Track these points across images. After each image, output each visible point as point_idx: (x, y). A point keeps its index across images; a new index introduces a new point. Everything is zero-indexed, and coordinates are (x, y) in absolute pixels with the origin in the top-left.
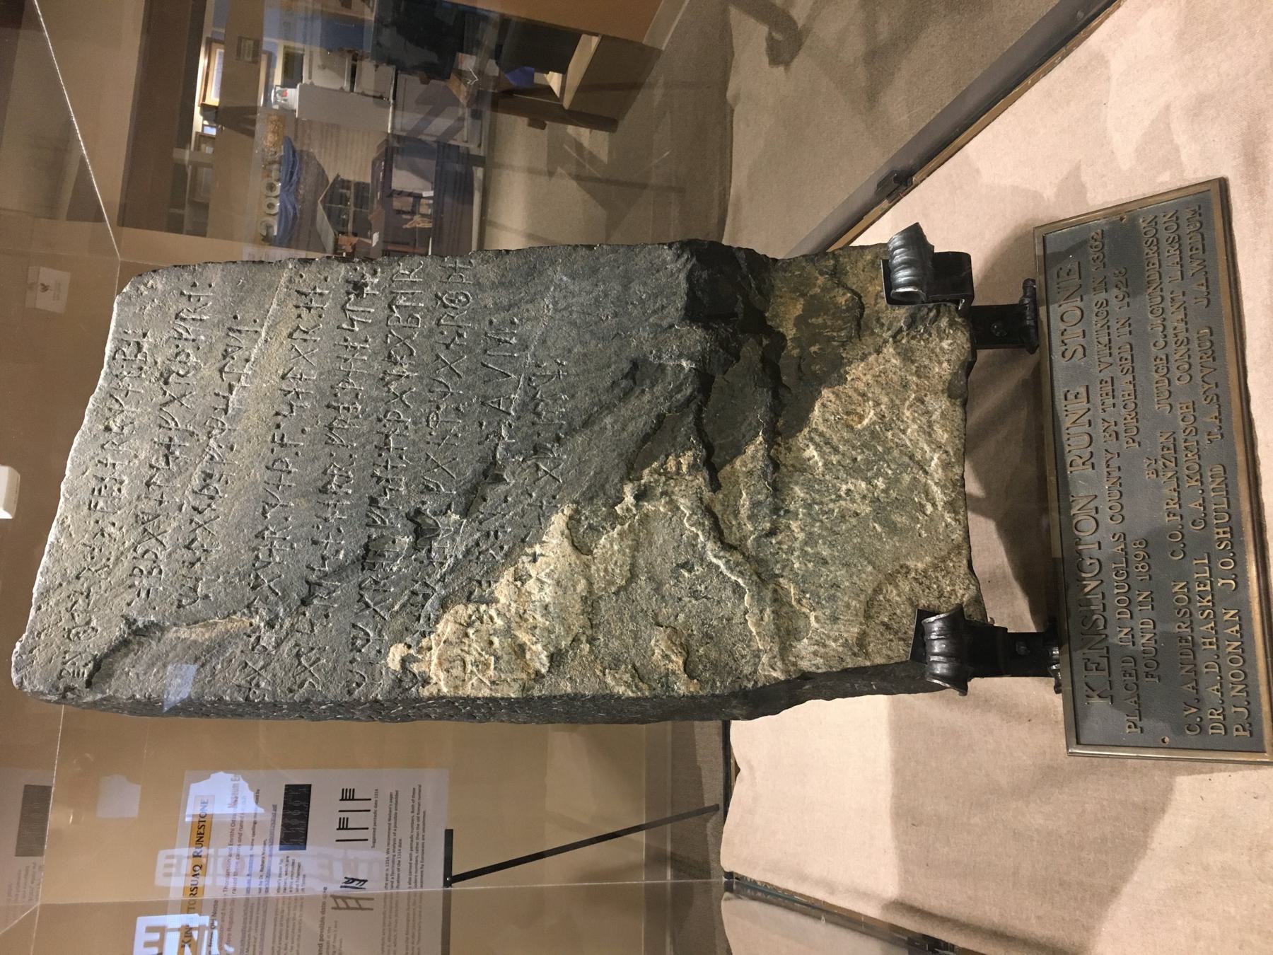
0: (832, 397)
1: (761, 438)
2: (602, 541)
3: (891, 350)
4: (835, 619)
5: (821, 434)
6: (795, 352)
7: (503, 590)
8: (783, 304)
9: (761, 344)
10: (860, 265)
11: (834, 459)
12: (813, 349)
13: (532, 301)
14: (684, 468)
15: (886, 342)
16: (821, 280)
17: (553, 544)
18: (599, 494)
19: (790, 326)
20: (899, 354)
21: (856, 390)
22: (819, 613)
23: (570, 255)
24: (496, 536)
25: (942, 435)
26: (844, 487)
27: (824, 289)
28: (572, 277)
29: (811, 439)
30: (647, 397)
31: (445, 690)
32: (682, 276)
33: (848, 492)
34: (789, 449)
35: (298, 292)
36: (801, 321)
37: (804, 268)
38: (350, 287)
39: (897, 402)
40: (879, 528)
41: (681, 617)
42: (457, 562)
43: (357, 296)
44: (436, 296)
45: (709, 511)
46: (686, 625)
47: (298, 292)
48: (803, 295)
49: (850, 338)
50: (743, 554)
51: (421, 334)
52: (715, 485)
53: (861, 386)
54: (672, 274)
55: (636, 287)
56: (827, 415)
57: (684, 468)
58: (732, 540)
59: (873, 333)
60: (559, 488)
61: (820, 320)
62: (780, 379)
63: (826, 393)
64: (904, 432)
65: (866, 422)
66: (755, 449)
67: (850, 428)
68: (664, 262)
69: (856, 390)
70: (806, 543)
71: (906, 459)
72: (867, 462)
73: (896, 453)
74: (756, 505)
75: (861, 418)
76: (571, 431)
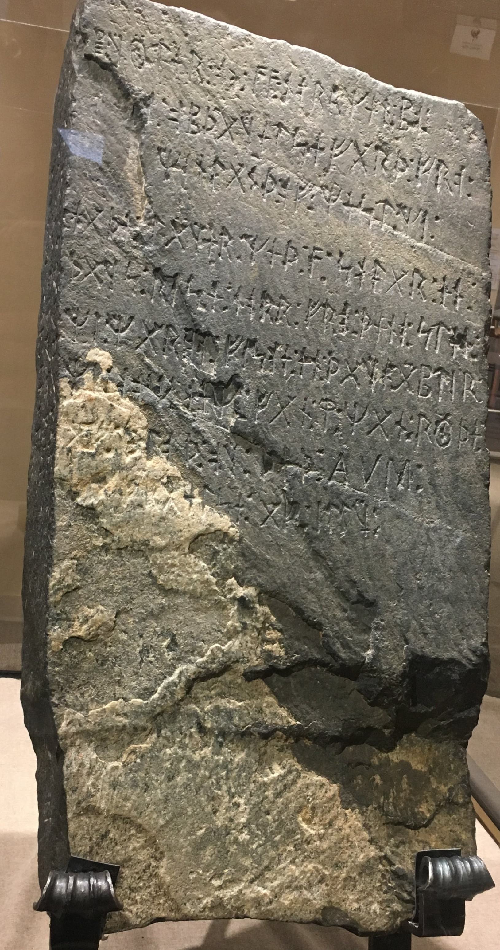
0: (330, 794)
1: (293, 722)
3: (373, 854)
4: (114, 785)
5: (294, 782)
7: (159, 464)
8: (423, 751)
14: (268, 647)
15: (381, 849)
16: (444, 789)
17: (201, 516)
19: (402, 757)
20: (369, 861)
21: (336, 818)
23: (481, 546)
25: (287, 899)
26: (242, 801)
27: (435, 792)
28: (460, 548)
29: (290, 772)
32: (454, 654)
33: (238, 805)
34: (281, 750)
36: (405, 767)
37: (457, 773)
39: (322, 857)
44: (448, 415)
45: (225, 668)
47: (459, 280)
48: (430, 771)
49: (386, 814)
50: (182, 700)
52: (251, 676)
53: (339, 823)
54: (457, 645)
59: (390, 836)
60: (256, 525)
61: (405, 786)
63: (334, 788)
64: (293, 862)
65: (304, 826)
66: (284, 717)
67: (299, 810)
68: (470, 638)
69: (336, 818)
70: (189, 761)
72: (265, 825)
74: (229, 714)
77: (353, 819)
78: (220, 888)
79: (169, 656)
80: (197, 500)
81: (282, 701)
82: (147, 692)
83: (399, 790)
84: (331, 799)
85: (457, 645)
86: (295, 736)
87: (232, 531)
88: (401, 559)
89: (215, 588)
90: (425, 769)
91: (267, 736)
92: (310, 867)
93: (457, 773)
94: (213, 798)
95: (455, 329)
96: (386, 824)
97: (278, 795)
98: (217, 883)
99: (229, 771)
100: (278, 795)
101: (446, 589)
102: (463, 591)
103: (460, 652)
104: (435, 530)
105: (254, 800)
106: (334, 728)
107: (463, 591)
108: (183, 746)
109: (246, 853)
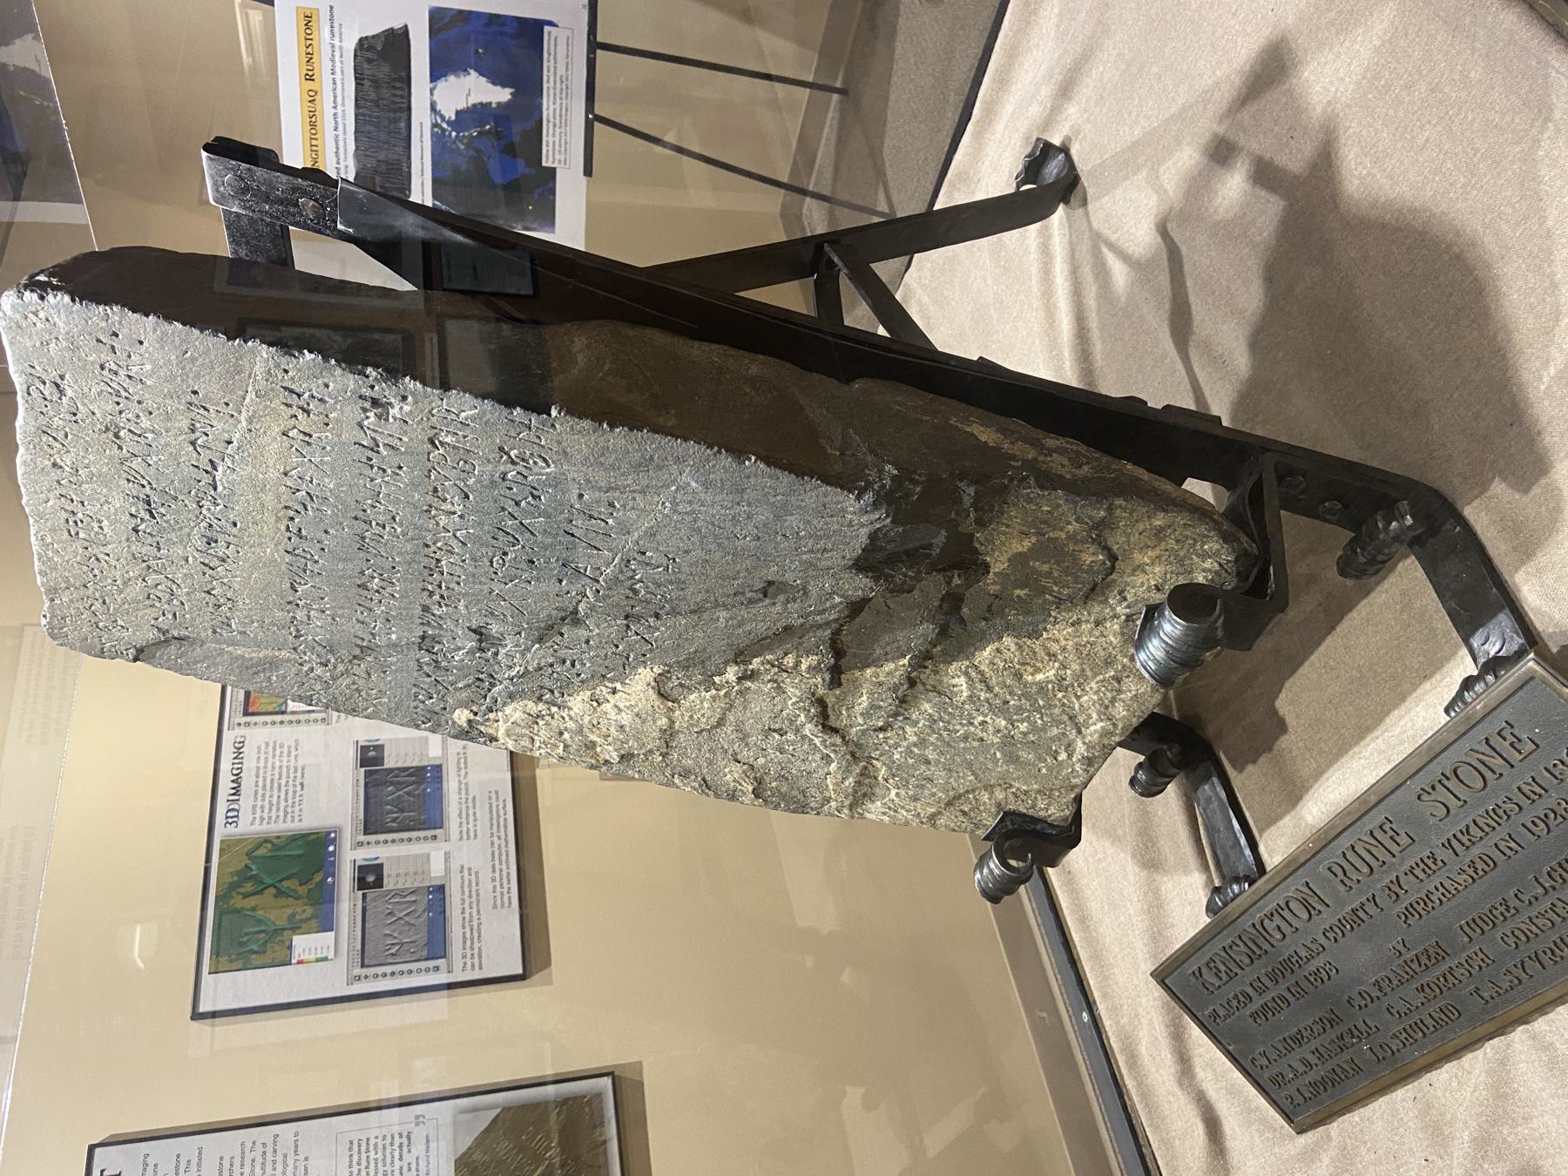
0: (1013, 647)
1: (906, 661)
2: (692, 697)
3: (1116, 627)
4: (915, 799)
5: (981, 673)
6: (994, 589)
7: (578, 703)
8: (1004, 533)
9: (949, 583)
10: (1141, 526)
11: (983, 696)
12: (1018, 592)
13: (643, 492)
14: (804, 667)
15: (1116, 616)
16: (1073, 527)
17: (640, 684)
18: (701, 668)
19: (1004, 558)
20: (1123, 634)
21: (1046, 648)
22: (902, 792)
23: (708, 461)
24: (573, 665)
25: (1120, 711)
26: (981, 718)
27: (1072, 537)
28: (707, 485)
29: (966, 674)
30: (779, 608)
31: (556, 383)
32: (864, 531)
33: (984, 723)
34: (936, 672)
35: (285, 388)
36: (1018, 560)
37: (1059, 506)
38: (367, 405)
39: (1089, 673)
40: (998, 755)
41: (761, 761)
42: (527, 672)
43: (379, 417)
44: (501, 449)
45: (821, 703)
46: (764, 766)
47: (285, 388)
48: (1039, 533)
49: (1071, 598)
50: (843, 738)
51: (479, 481)
52: (835, 682)
53: (1055, 647)
54: (850, 525)
55: (793, 520)
56: (997, 660)
57: (804, 667)
58: (832, 722)
59: (1106, 601)
60: (651, 651)
61: (1046, 567)
62: (959, 608)
63: (1008, 641)
64: (1078, 698)
65: (1040, 677)
66: (894, 669)
67: (1018, 676)
68: (844, 510)
69: (1046, 648)
70: (915, 745)
71: (1065, 718)
72: (1020, 709)
73: (1057, 711)
74: (873, 707)
75: (1038, 670)
76: (674, 612)
77: (1060, 634)
78: (1070, 756)
79: (791, 736)
80: (618, 686)
81: (877, 663)
82: (827, 759)
83: (1049, 574)
84: (1020, 647)
85: (850, 525)
86: (923, 659)
87: (657, 670)
88: (713, 547)
89: (722, 693)
90: (1034, 540)
91: (912, 683)
92: (1093, 685)
93: (1059, 506)
94: (965, 738)
95: (365, 410)
96: (1163, 231)
97: (989, 689)
98: (1063, 756)
99: (941, 719)
100: (989, 689)
101: (763, 515)
102: (772, 500)
103: (862, 525)
104: (675, 504)
105: (985, 709)
106: (928, 629)
107: (772, 500)
108: (897, 745)
109: (1044, 729)
